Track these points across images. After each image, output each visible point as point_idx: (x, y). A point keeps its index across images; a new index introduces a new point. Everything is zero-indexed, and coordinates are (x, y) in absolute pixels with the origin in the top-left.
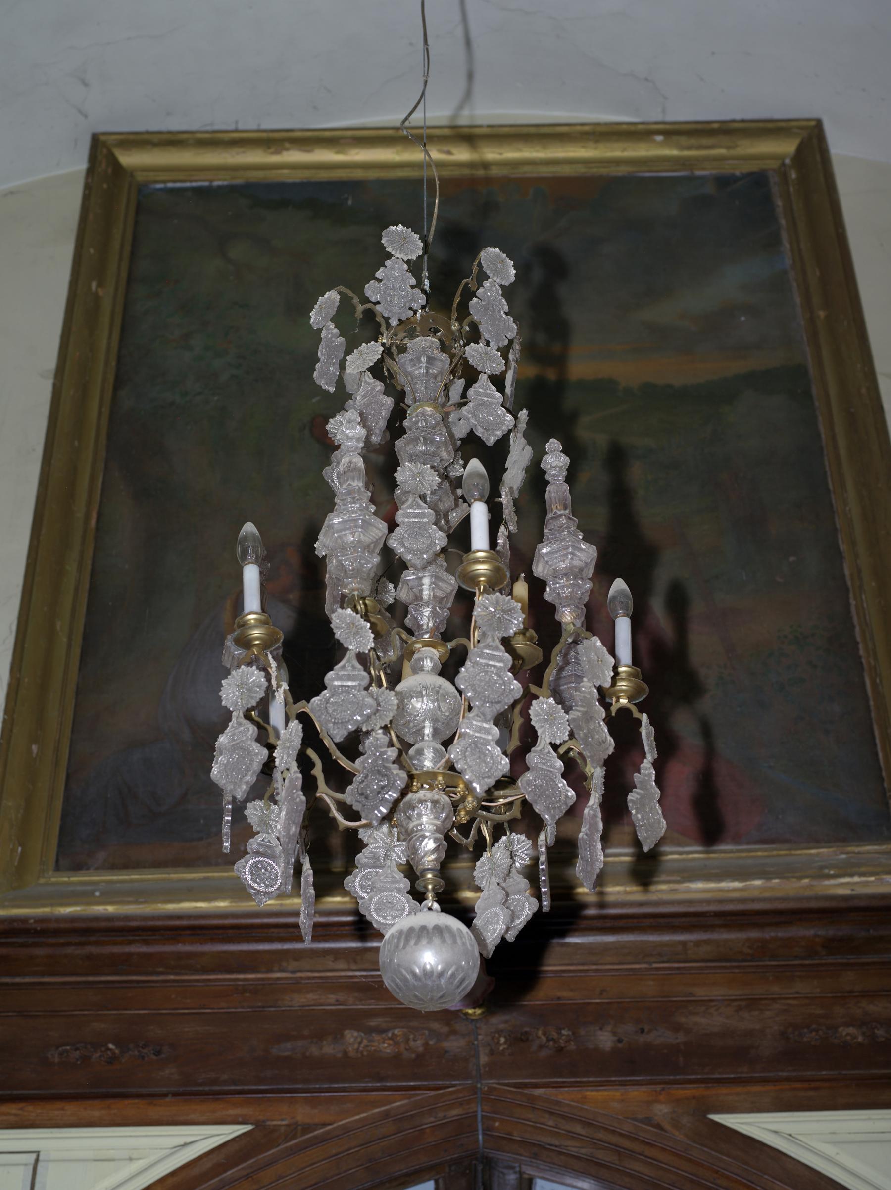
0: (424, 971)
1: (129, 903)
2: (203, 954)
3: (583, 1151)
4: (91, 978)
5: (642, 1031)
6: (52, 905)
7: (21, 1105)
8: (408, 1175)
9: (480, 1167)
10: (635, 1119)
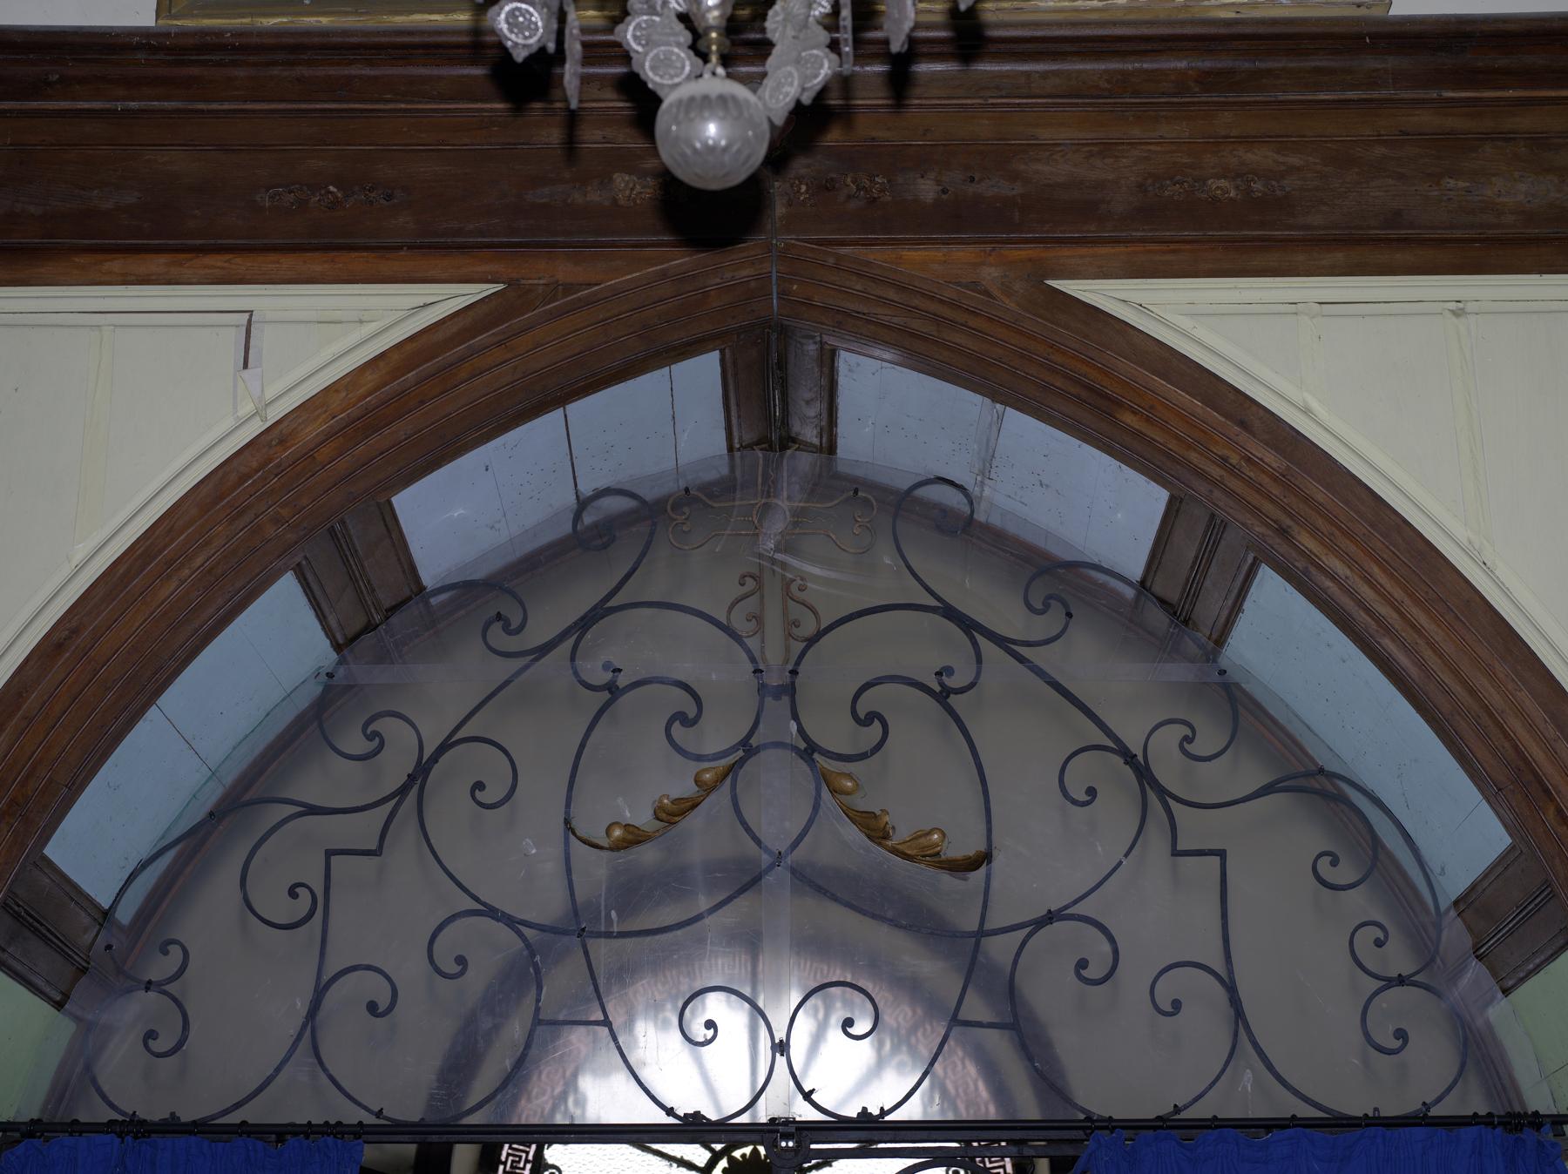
0: (705, 145)
1: (347, 13)
2: (440, 78)
3: (895, 320)
4: (304, 106)
5: (972, 180)
6: (252, 15)
7: (228, 257)
8: (689, 344)
9: (774, 337)
10: (958, 284)
